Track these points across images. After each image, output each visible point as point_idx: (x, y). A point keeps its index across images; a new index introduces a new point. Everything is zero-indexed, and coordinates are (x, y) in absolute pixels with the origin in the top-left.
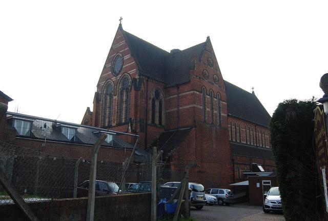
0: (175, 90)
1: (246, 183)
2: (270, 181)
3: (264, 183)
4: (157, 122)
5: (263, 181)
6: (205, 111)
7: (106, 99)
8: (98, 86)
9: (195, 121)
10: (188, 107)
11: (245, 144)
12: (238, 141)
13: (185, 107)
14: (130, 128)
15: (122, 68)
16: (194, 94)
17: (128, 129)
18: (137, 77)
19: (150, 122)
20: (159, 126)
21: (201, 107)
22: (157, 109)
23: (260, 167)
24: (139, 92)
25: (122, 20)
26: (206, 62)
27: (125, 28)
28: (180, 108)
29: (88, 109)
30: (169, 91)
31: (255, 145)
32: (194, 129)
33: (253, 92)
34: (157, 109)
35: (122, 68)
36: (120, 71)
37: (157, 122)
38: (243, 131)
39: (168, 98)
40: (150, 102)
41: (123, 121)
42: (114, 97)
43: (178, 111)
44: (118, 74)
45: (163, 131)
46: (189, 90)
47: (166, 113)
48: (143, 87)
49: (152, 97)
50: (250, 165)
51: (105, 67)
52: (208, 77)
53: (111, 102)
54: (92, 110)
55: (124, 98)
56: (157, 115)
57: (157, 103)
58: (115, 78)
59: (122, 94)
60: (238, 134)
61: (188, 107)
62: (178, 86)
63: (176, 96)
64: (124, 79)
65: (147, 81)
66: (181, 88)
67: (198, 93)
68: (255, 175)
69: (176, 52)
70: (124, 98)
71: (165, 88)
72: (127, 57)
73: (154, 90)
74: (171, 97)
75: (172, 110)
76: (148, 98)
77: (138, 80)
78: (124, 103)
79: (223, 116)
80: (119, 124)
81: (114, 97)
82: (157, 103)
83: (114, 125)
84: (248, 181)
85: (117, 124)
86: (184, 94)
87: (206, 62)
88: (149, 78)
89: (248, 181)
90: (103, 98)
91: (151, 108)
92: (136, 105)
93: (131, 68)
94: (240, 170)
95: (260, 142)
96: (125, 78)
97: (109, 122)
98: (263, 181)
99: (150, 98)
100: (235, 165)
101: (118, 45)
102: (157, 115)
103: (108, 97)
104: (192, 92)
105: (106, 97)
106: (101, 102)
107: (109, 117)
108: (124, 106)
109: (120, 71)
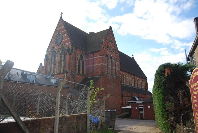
0: (91, 55)
1: (130, 107)
2: (143, 106)
3: (140, 107)
4: (81, 72)
5: (139, 106)
7: (52, 59)
8: (47, 51)
10: (99, 64)
11: (128, 85)
12: (123, 83)
13: (98, 65)
14: (66, 75)
15: (61, 42)
16: (102, 58)
17: (65, 76)
18: (70, 47)
19: (77, 72)
21: (106, 65)
22: (81, 65)
23: (137, 98)
24: (72, 55)
25: (62, 14)
26: (109, 40)
27: (64, 19)
28: (94, 65)
29: (41, 64)
30: (88, 55)
32: (102, 77)
33: (133, 57)
34: (81, 65)
35: (61, 42)
36: (60, 43)
37: (81, 72)
39: (88, 59)
40: (78, 61)
41: (62, 72)
42: (57, 58)
43: (93, 67)
44: (59, 45)
45: (84, 77)
46: (99, 55)
47: (86, 68)
48: (73, 53)
50: (131, 97)
51: (51, 41)
52: (110, 48)
54: (43, 65)
55: (63, 59)
56: (81, 68)
57: (81, 62)
59: (61, 56)
60: (125, 80)
61: (99, 64)
62: (93, 53)
63: (92, 58)
64: (63, 48)
65: (76, 49)
66: (95, 54)
67: (104, 57)
68: (136, 102)
69: (92, 34)
70: (63, 59)
72: (64, 35)
73: (80, 54)
74: (89, 59)
77: (71, 49)
79: (114, 69)
80: (60, 73)
81: (57, 58)
82: (81, 62)
85: (58, 73)
86: (97, 57)
87: (109, 40)
88: (77, 48)
91: (78, 65)
92: (70, 63)
93: (67, 41)
95: (137, 84)
96: (64, 47)
97: (54, 72)
98: (139, 106)
99: (77, 59)
100: (124, 97)
101: (60, 29)
102: (81, 68)
103: (63, 56)
105: (52, 57)
107: (54, 69)
108: (62, 63)
109: (60, 43)
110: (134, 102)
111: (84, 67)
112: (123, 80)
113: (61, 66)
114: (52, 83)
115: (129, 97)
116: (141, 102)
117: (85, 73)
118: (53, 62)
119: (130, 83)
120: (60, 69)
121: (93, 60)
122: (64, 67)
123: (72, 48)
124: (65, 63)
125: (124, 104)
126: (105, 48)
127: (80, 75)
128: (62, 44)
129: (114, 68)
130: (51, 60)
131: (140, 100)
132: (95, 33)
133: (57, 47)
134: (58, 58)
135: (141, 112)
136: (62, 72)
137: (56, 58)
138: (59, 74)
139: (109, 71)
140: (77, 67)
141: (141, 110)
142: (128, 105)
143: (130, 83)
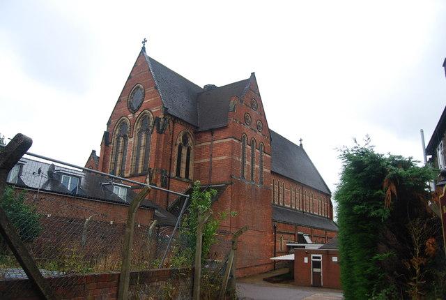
0: (208, 136)
1: (291, 257)
2: (321, 256)
3: (314, 257)
4: (183, 174)
5: (312, 255)
6: (261, 172)
7: (118, 142)
8: (109, 124)
9: (231, 176)
12: (294, 208)
16: (232, 142)
18: (161, 116)
19: (174, 174)
20: (185, 180)
22: (184, 158)
23: (307, 238)
27: (150, 53)
29: (94, 152)
30: (201, 137)
31: (301, 210)
33: (301, 145)
34: (184, 158)
35: (141, 104)
36: (139, 108)
37: (183, 174)
38: (287, 192)
40: (176, 149)
41: (140, 172)
42: (130, 140)
43: (210, 163)
44: (134, 112)
49: (178, 143)
50: (294, 235)
53: (125, 146)
54: (98, 154)
55: (143, 142)
56: (183, 166)
57: (184, 151)
58: (132, 115)
60: (281, 196)
62: (212, 131)
63: (210, 143)
64: (144, 118)
66: (216, 134)
67: (236, 141)
68: (304, 247)
69: (210, 88)
70: (143, 142)
71: (195, 133)
73: (182, 134)
74: (202, 144)
75: (202, 161)
76: (174, 144)
78: (142, 148)
79: (266, 172)
81: (130, 140)
82: (184, 151)
83: (126, 175)
84: (293, 255)
86: (220, 141)
89: (293, 255)
90: (114, 140)
92: (157, 153)
94: (283, 241)
95: (308, 206)
96: (124, 123)
97: (122, 171)
98: (312, 255)
102: (183, 166)
103: (122, 139)
104: (230, 139)
105: (118, 138)
106: (112, 145)
108: (142, 151)
110: (300, 247)
111: (191, 163)
112: (276, 195)
113: (137, 159)
114: (116, 196)
115: (288, 233)
116: (316, 247)
117: (191, 177)
118: (120, 149)
119: (293, 202)
120: (137, 165)
121: (211, 146)
122: (145, 162)
123: (165, 119)
124: (147, 150)
125: (278, 249)
126: (240, 123)
127: (180, 179)
128: (142, 108)
129: (257, 166)
130: (115, 144)
131: (315, 242)
132: (273, 125)
133: (130, 116)
134: (132, 140)
135: (316, 270)
136: (140, 172)
137: (127, 140)
138: (132, 176)
139: (245, 174)
140: (175, 162)
141: (317, 265)
142: (288, 253)
143: (293, 202)
